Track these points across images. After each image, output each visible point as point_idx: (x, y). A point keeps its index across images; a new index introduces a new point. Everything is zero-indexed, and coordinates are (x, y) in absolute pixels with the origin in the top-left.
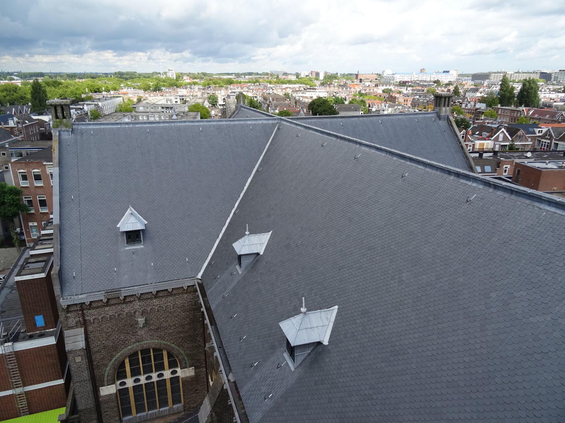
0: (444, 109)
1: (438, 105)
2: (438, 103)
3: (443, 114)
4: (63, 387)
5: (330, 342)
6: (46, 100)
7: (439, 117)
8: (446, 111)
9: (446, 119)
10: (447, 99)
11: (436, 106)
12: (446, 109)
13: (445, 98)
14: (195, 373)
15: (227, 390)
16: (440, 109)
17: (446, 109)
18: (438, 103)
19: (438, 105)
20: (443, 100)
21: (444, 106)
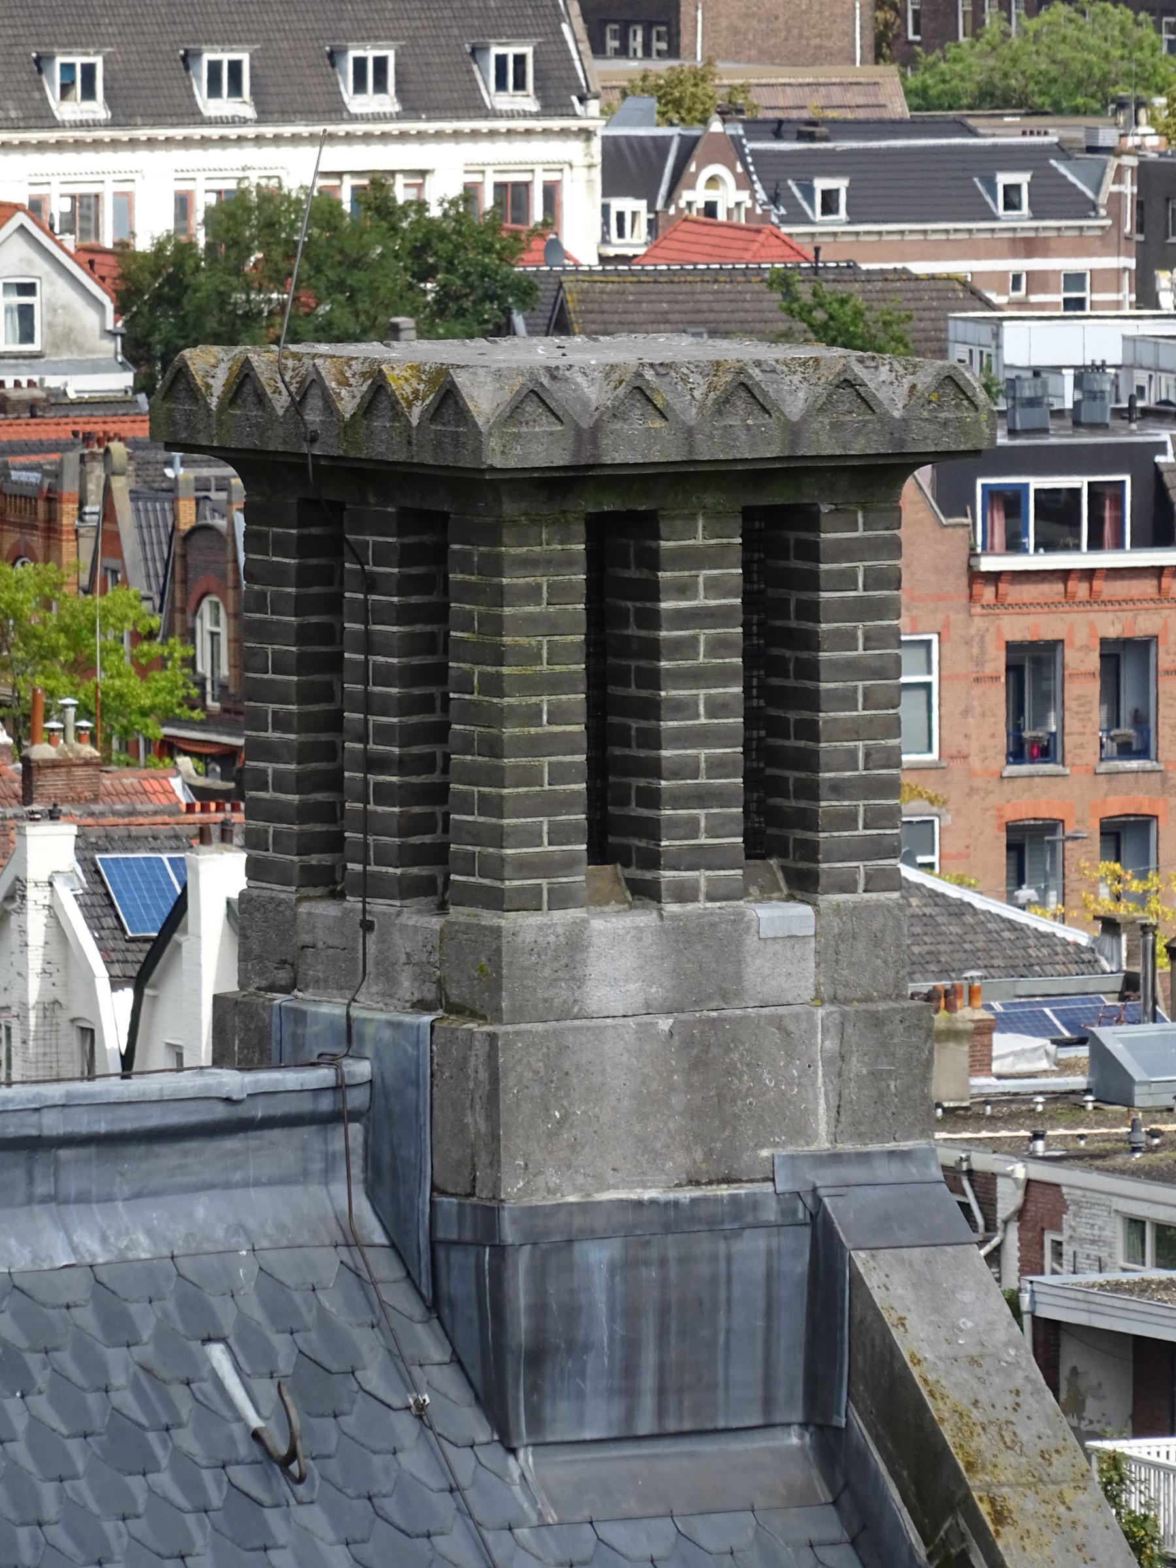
0: (608, 962)
1: (376, 809)
2: (376, 727)
3: (589, 1163)
4: (467, 462)
5: (147, 1441)
6: (865, 510)
7: (464, 1282)
8: (710, 1050)
9: (757, 1346)
10: (700, 587)
11: (309, 852)
12: (705, 973)
13: (618, 518)
14: (893, 62)
15: (116, 984)
16: (466, 990)
17: (705, 973)
18: (376, 727)
19: (376, 809)
20: (540, 597)
21: (621, 839)
